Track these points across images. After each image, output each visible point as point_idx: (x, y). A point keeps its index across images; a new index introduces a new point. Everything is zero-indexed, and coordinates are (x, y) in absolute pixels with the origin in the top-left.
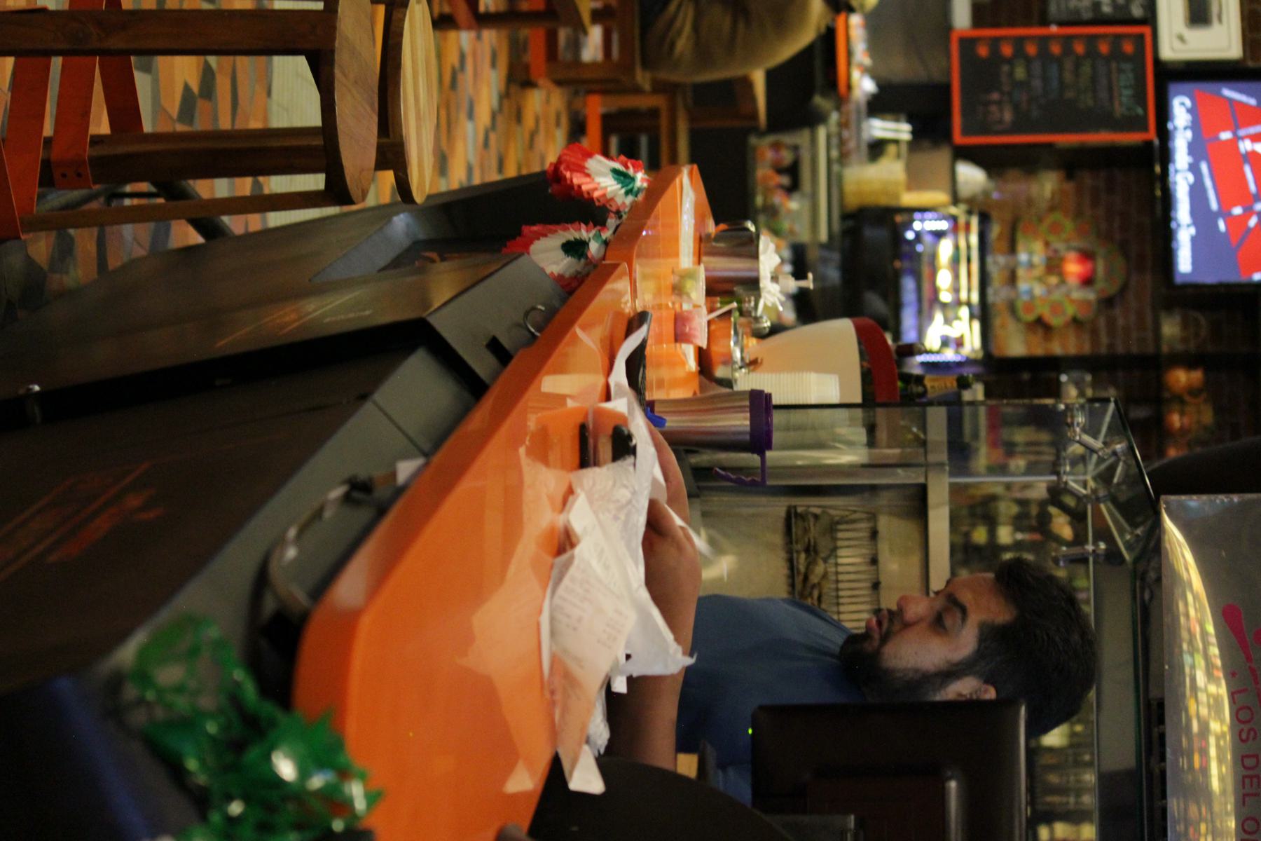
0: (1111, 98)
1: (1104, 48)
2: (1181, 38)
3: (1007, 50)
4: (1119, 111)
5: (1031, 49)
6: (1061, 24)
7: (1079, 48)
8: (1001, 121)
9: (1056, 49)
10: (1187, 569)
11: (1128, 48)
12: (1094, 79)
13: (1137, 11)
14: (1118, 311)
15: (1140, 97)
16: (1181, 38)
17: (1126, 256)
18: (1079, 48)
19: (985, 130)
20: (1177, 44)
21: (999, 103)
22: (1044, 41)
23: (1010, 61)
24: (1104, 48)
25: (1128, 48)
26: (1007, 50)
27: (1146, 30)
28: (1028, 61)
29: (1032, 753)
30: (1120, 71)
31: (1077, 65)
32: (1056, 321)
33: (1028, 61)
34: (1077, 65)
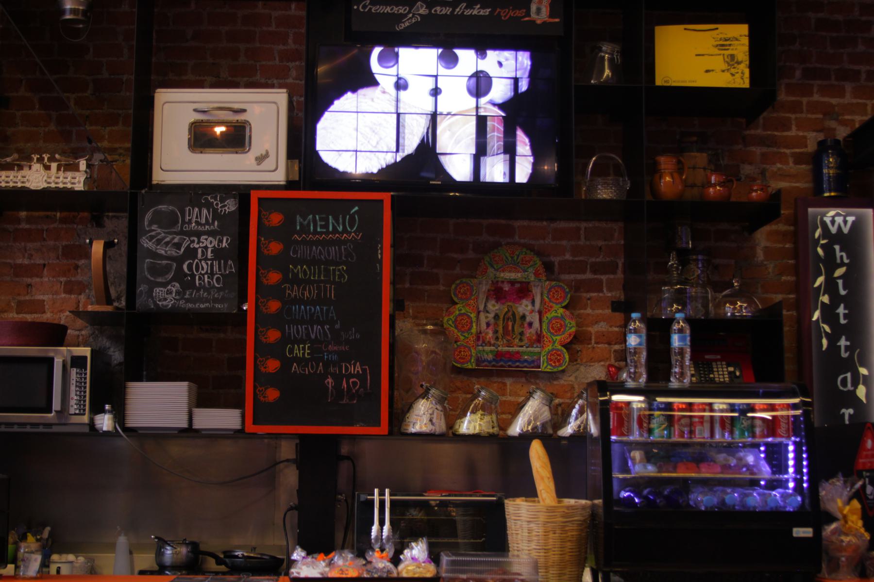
0: (339, 243)
1: (275, 248)
2: (260, 159)
3: (273, 365)
4: (353, 234)
5: (273, 335)
6: (243, 298)
7: (274, 277)
8: (361, 377)
9: (274, 306)
10: (11, 425)
11: (276, 219)
12: (313, 262)
13: (231, 206)
14: (556, 260)
15: (340, 208)
16: (260, 159)
17: (496, 245)
18: (274, 277)
19: (373, 396)
20: (269, 164)
21: (338, 378)
22: (262, 320)
23: (286, 363)
24: (275, 248)
25: (276, 219)
26: (273, 365)
27: (255, 196)
28: (286, 340)
29: (278, 436)
30: (305, 229)
31: (296, 281)
32: (571, 327)
33: (286, 340)
34: (296, 281)
